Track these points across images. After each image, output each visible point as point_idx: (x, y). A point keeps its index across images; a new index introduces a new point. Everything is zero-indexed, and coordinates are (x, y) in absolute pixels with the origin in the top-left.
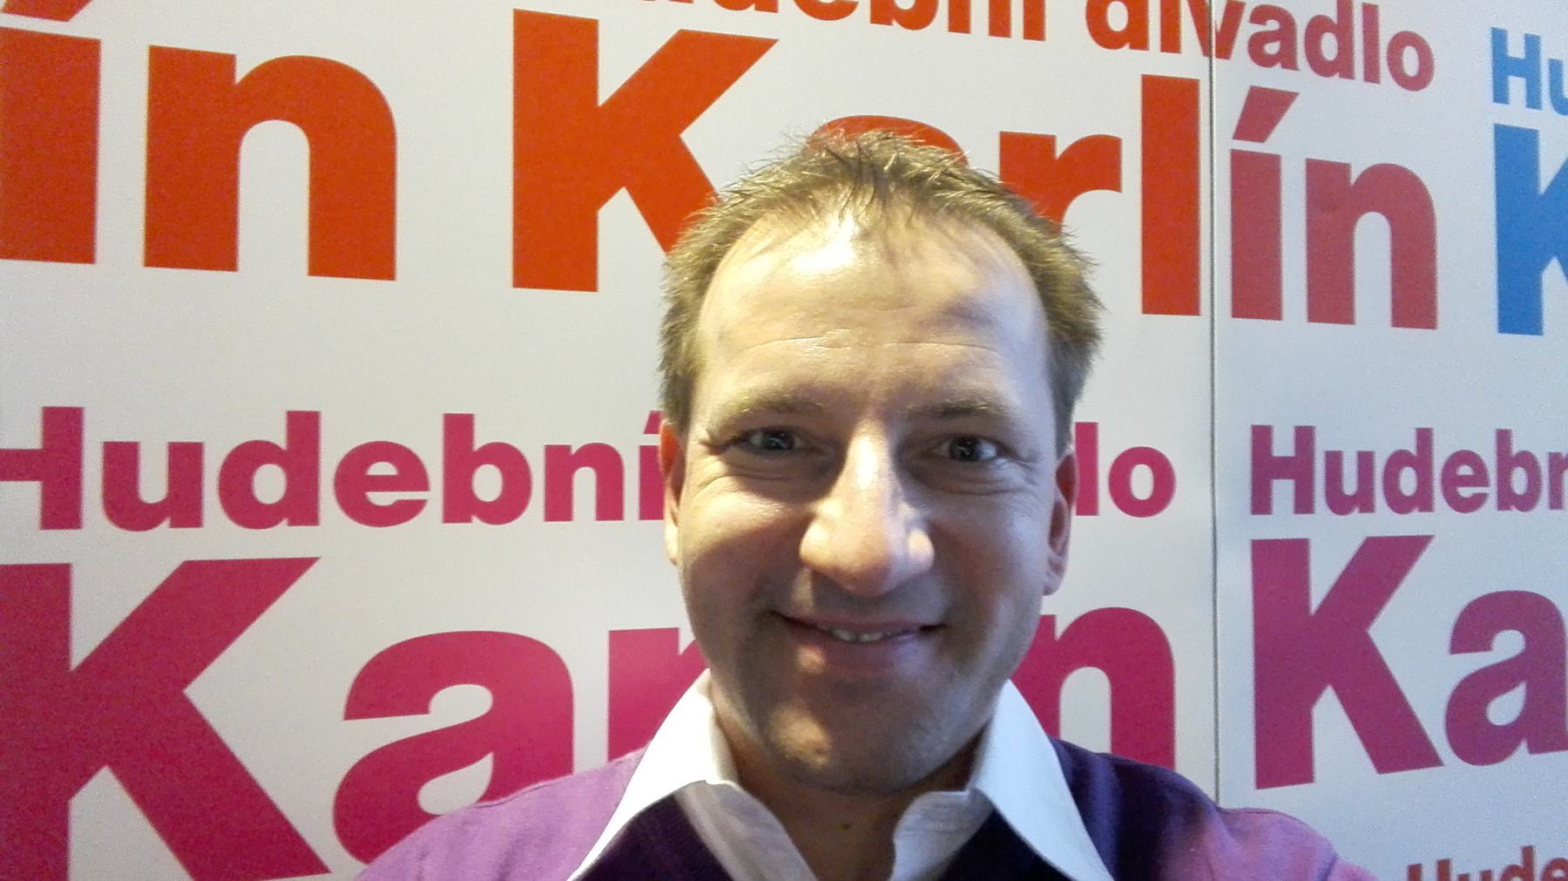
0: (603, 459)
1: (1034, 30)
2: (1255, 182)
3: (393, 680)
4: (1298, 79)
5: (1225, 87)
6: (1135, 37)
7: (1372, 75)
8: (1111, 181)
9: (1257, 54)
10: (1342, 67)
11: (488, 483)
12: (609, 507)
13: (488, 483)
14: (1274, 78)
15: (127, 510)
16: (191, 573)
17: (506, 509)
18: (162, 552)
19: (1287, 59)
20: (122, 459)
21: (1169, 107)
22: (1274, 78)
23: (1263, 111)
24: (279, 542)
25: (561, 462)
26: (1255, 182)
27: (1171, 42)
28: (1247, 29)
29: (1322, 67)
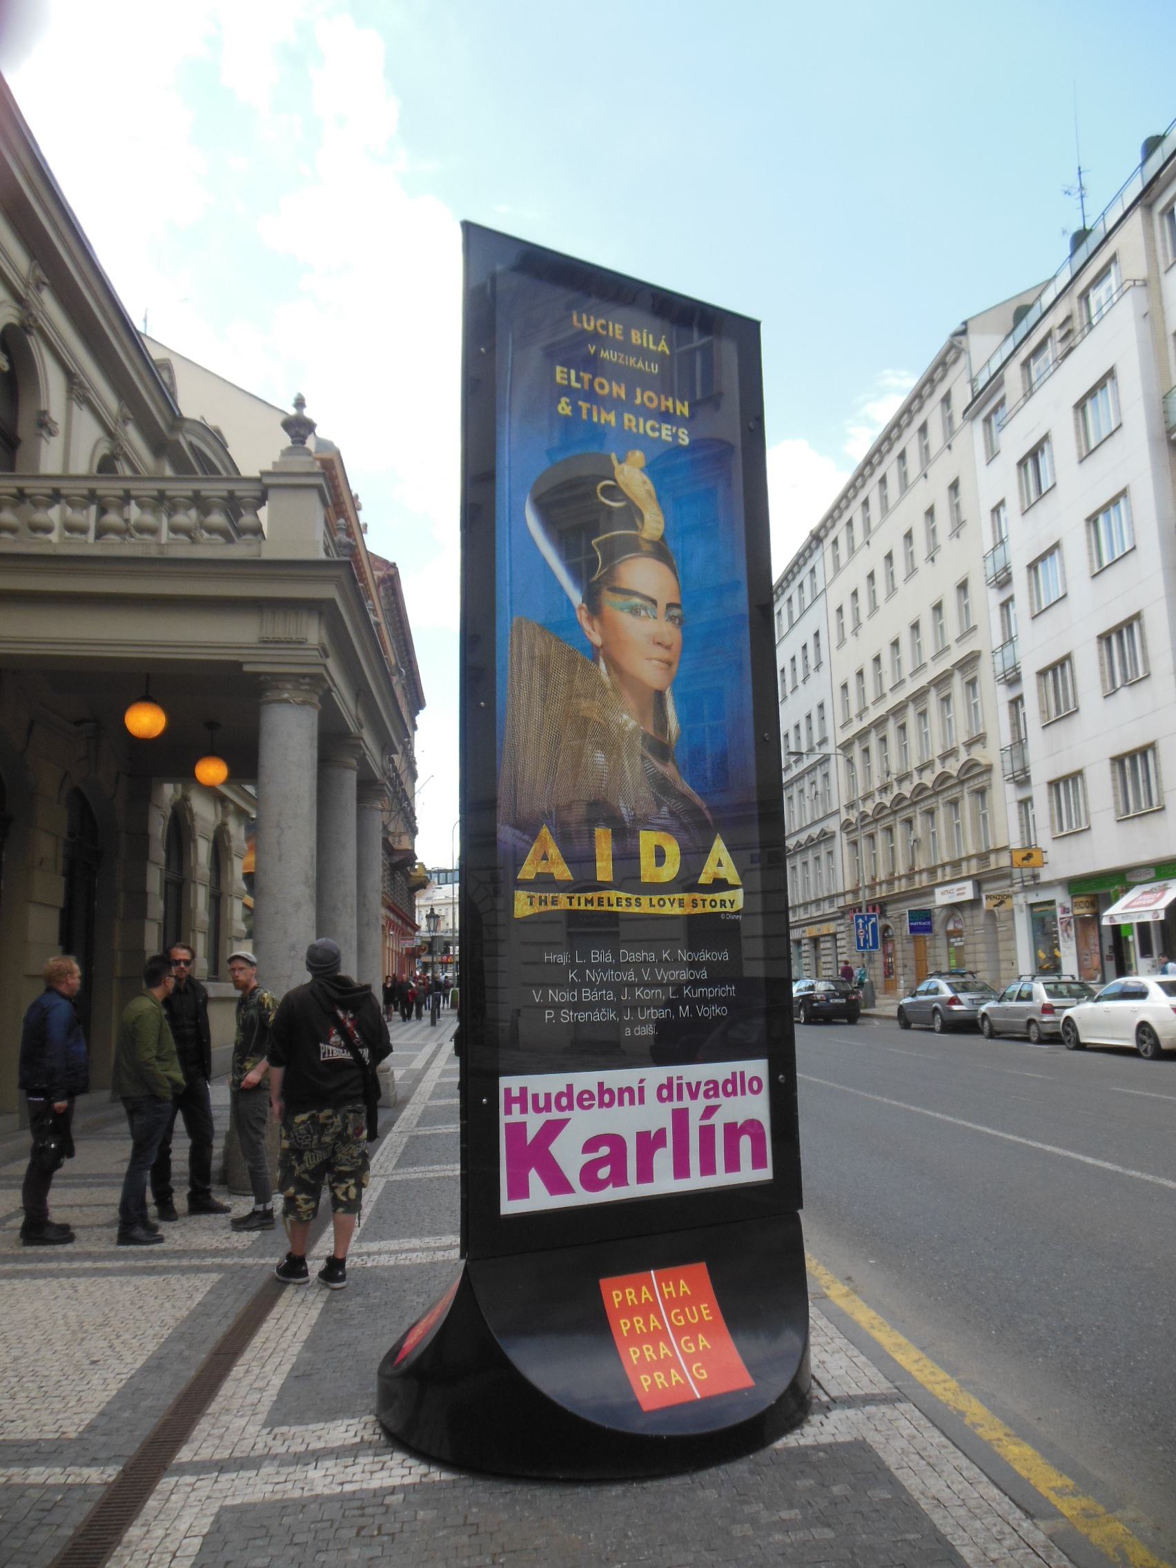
0: (630, 1090)
1: (642, 1101)
2: (707, 1134)
3: (591, 1145)
4: (722, 1100)
5: (696, 1108)
6: (670, 1098)
7: (743, 1093)
8: (664, 1144)
9: (706, 1095)
10: (734, 1093)
11: (607, 1098)
12: (632, 1102)
13: (607, 1098)
14: (713, 1102)
15: (537, 1110)
16: (548, 1122)
17: (610, 1104)
18: (546, 1116)
19: (716, 1095)
20: (536, 1097)
21: (680, 1117)
22: (713, 1102)
23: (709, 1111)
24: (565, 1115)
25: (621, 1091)
26: (707, 1134)
27: (680, 1098)
28: (703, 1088)
29: (727, 1094)
